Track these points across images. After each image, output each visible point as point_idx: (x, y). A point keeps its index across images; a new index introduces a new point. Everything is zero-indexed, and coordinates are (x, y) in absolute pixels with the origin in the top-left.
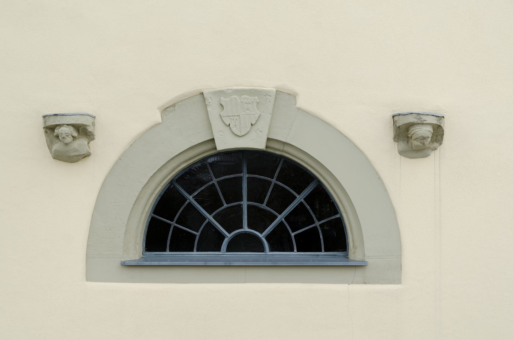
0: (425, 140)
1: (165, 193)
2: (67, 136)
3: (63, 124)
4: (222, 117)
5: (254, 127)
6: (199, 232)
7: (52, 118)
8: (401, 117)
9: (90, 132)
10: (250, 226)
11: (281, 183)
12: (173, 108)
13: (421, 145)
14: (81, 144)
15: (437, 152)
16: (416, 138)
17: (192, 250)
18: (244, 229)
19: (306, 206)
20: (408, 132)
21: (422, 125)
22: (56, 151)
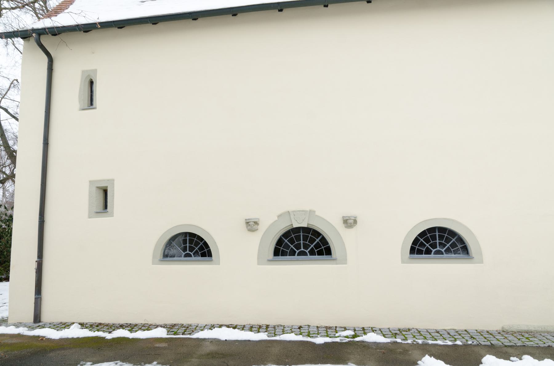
1: (279, 239)
10: (303, 248)
14: (256, 226)
15: (356, 227)
17: (423, 254)
22: (249, 229)
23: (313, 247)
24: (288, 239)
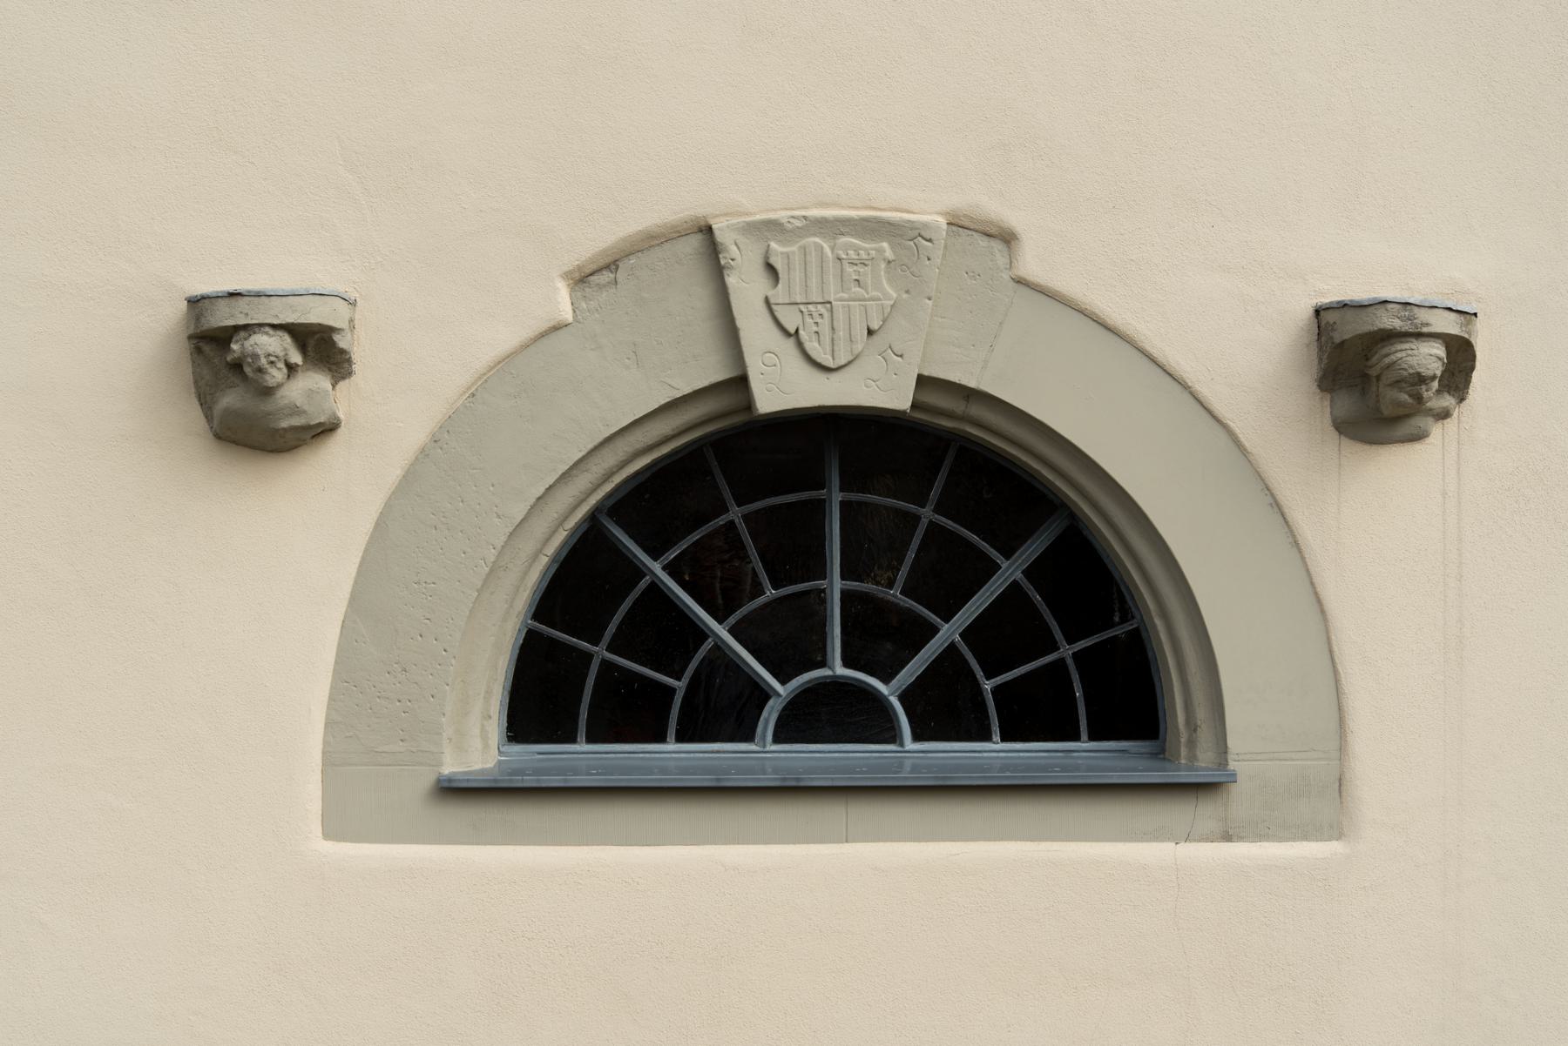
0: (1424, 387)
2: (272, 362)
3: (261, 325)
4: (773, 306)
5: (875, 337)
6: (683, 679)
7: (222, 302)
8: (1349, 314)
9: (343, 352)
11: (950, 522)
12: (612, 276)
13: (1410, 400)
15: (1450, 424)
16: (1398, 378)
17: (660, 738)
18: (830, 668)
19: (1030, 593)
20: (1367, 360)
21: (1416, 339)
22: (229, 413)
23: (952, 646)
24: (672, 554)
